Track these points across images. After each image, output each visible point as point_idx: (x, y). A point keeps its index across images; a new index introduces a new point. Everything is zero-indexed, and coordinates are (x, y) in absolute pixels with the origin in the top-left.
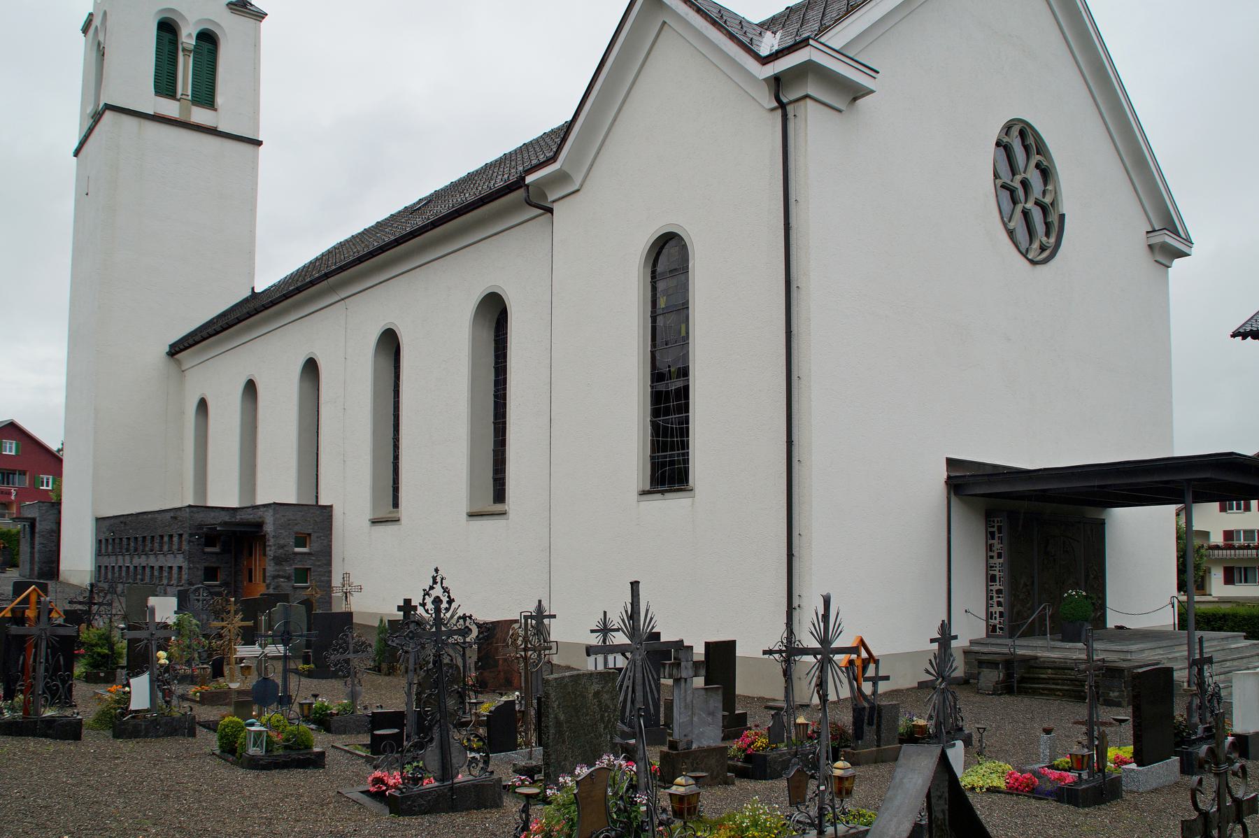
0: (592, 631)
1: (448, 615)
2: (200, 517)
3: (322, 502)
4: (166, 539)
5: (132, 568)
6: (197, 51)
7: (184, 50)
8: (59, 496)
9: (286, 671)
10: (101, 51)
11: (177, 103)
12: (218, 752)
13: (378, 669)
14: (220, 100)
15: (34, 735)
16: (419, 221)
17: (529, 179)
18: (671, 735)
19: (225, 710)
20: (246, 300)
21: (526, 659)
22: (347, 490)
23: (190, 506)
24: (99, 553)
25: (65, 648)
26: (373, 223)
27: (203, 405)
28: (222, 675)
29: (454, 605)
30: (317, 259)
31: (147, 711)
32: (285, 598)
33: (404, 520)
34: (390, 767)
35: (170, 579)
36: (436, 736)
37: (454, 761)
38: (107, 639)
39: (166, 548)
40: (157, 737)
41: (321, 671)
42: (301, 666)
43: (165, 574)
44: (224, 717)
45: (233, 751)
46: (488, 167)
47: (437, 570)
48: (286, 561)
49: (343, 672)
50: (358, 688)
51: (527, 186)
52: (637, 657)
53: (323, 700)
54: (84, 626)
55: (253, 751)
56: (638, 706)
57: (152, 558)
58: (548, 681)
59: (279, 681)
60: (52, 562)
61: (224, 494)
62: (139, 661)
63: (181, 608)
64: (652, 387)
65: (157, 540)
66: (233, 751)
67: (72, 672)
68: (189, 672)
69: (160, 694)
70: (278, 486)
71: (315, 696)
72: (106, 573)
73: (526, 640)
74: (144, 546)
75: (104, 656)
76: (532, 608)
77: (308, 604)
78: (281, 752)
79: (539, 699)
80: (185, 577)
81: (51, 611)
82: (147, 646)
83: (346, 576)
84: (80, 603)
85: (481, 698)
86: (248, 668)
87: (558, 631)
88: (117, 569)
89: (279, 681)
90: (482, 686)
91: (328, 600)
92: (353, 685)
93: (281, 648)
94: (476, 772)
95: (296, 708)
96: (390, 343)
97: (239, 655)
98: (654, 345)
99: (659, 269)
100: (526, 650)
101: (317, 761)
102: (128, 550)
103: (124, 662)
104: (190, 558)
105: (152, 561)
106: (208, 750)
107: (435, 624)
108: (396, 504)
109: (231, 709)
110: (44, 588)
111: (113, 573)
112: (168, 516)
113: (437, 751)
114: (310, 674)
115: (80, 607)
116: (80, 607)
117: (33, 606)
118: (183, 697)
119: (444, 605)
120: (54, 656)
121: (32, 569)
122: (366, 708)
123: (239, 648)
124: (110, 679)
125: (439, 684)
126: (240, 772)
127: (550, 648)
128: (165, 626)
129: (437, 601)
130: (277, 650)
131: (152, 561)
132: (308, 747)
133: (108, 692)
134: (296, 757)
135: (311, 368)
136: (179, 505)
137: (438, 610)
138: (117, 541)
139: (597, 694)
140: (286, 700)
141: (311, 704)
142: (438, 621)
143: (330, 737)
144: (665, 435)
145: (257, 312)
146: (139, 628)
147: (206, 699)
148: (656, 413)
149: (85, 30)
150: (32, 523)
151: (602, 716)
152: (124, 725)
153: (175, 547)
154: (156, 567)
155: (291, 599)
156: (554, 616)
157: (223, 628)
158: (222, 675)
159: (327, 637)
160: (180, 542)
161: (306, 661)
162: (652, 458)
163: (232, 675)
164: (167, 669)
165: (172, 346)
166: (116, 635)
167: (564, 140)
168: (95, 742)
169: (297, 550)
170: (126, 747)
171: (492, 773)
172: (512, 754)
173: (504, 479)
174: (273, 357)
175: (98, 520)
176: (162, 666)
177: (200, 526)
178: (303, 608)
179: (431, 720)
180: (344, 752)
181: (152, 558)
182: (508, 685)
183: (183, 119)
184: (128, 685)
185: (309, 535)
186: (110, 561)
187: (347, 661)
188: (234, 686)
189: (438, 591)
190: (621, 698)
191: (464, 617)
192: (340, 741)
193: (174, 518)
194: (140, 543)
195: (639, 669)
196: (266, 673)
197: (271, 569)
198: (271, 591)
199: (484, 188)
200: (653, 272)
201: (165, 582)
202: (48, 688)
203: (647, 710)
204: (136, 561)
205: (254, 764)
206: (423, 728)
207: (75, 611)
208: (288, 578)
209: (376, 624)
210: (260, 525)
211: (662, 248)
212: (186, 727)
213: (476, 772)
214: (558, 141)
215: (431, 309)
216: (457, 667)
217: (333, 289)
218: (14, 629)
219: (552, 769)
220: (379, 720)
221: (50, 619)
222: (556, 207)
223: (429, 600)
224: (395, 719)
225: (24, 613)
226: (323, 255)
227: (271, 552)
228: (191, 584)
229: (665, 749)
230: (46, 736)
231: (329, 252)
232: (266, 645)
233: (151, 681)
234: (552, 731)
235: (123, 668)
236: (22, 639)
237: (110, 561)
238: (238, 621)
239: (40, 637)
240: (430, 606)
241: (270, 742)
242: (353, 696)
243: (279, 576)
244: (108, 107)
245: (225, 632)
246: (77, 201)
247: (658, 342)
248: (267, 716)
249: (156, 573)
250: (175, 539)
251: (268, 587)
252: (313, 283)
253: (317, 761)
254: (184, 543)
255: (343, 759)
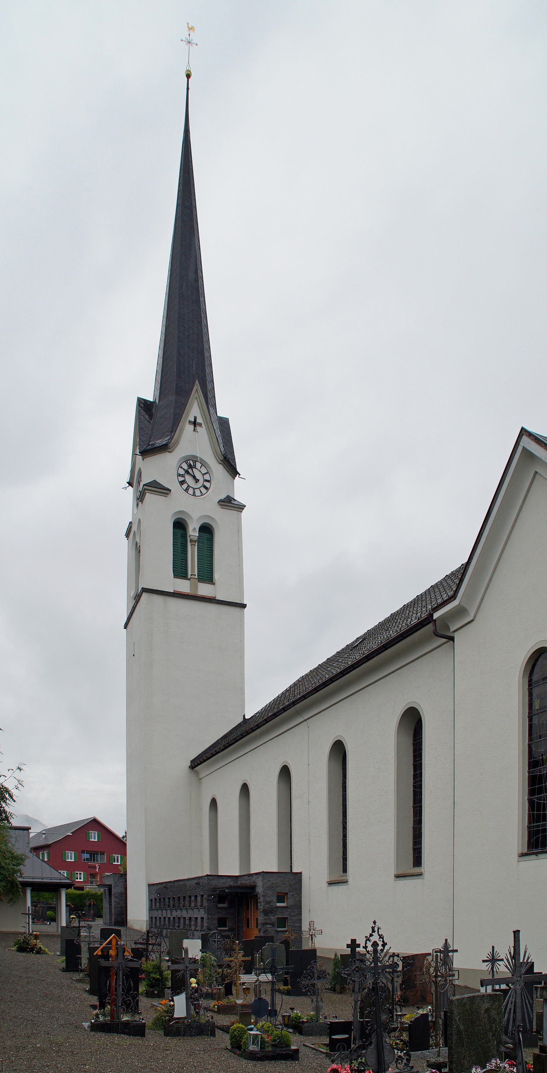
0: (484, 961)
1: (383, 954)
2: (215, 883)
3: (295, 870)
4: (193, 898)
5: (172, 919)
6: (200, 540)
7: (191, 541)
8: (125, 869)
9: (273, 991)
10: (137, 549)
11: (189, 581)
12: (229, 1048)
13: (333, 990)
14: (216, 576)
15: (117, 1033)
16: (358, 656)
17: (436, 616)
18: (541, 1039)
19: (234, 1018)
20: (240, 725)
21: (436, 983)
22: (312, 862)
23: (207, 875)
24: (151, 909)
25: (133, 975)
26: (325, 660)
27: (214, 803)
28: (231, 994)
29: (387, 947)
30: (287, 691)
31: (185, 1018)
32: (271, 939)
33: (350, 881)
34: (343, 1060)
35: (196, 926)
36: (374, 1040)
37: (386, 1058)
38: (158, 968)
39: (193, 904)
40: (191, 1036)
41: (295, 991)
42: (282, 987)
43: (193, 923)
44: (233, 1024)
45: (239, 1047)
46: (405, 607)
47: (375, 922)
48: (271, 913)
49: (311, 991)
50: (321, 1004)
51: (435, 621)
52: (518, 987)
53: (297, 1012)
54: (144, 959)
55: (252, 1048)
56: (518, 1024)
57: (184, 911)
58: (452, 1001)
59: (268, 999)
60: (123, 914)
61: (230, 867)
62: (179, 985)
63: (204, 948)
64: (529, 772)
65: (187, 899)
66: (239, 1047)
67: (138, 991)
68: (210, 991)
69: (192, 1007)
70: (265, 860)
71: (292, 1009)
72: (156, 922)
73: (436, 970)
74: (179, 903)
75: (157, 980)
76: (440, 946)
77: (286, 943)
78: (270, 1049)
79: (445, 1013)
80: (205, 924)
81: (124, 952)
82: (183, 975)
83: (311, 923)
84: (141, 944)
85: (405, 1011)
86: (248, 989)
87: (458, 962)
88: (162, 919)
89: (268, 999)
90: (405, 1002)
91: (299, 940)
92: (317, 1001)
93: (270, 977)
94: (401, 1066)
95: (280, 1018)
96: (339, 751)
97: (242, 981)
98: (530, 739)
99: (535, 678)
100: (436, 976)
101: (293, 1056)
102: (169, 906)
103: (169, 984)
104: (208, 912)
105: (185, 914)
106: (223, 1046)
107: (373, 961)
108: (345, 870)
109: (238, 1018)
110: (118, 933)
111: (160, 922)
112: (194, 882)
113: (375, 1051)
114: (288, 993)
115: (141, 946)
116: (141, 946)
117: (114, 948)
118: (207, 1009)
119: (380, 948)
120: (127, 979)
121: (111, 919)
122: (325, 1018)
123: (242, 976)
124: (161, 995)
125: (376, 1002)
126: (244, 1062)
127: (454, 975)
128: (194, 961)
129: (375, 944)
130: (266, 977)
131: (185, 914)
132: (288, 1046)
133: (160, 1004)
134: (281, 1053)
135: (285, 772)
136: (200, 875)
137: (375, 951)
138: (162, 900)
139: (487, 1010)
140: (273, 1013)
141: (289, 1016)
142: (376, 959)
143: (302, 1038)
144: (538, 810)
145: (248, 733)
146: (178, 963)
147: (222, 1010)
148: (532, 792)
149: (127, 535)
150: (110, 887)
151: (491, 1027)
152: (171, 1027)
153: (199, 904)
154: (187, 918)
155: (275, 939)
156: (456, 951)
157: (231, 961)
158: (231, 994)
159: (299, 968)
160: (202, 900)
161: (286, 984)
162: (529, 827)
163: (238, 994)
164: (196, 990)
165: (192, 762)
166: (164, 965)
167: (461, 580)
168: (154, 1038)
169: (279, 904)
170: (173, 1042)
171: (412, 1067)
172: (426, 1052)
173: (421, 848)
174: (257, 766)
175: (150, 885)
176: (193, 988)
177: (215, 889)
178: (283, 946)
179: (371, 1030)
180: (309, 1046)
181: (184, 911)
182: (423, 1001)
183: (193, 593)
184: (173, 1000)
185: (287, 894)
186: (158, 914)
187: (313, 985)
188: (239, 1002)
189: (375, 938)
190: (506, 1018)
191: (393, 955)
192: (309, 1041)
193: (198, 884)
194: (176, 901)
195: (519, 996)
196: (260, 995)
197: (261, 918)
198: (262, 934)
199: (403, 626)
200: (530, 681)
201: (193, 928)
202: (125, 1002)
203: (524, 1026)
204: (175, 914)
205: (252, 1057)
206: (364, 1035)
207: (138, 949)
208: (273, 925)
209: (333, 957)
210: (253, 887)
211: (536, 660)
212: (208, 1030)
213: (401, 1066)
214: (457, 581)
215: (366, 722)
216: (388, 988)
217: (298, 713)
218: (103, 963)
219: (454, 1065)
220: (334, 1028)
221: (124, 956)
222: (457, 636)
223: (369, 944)
224: (345, 1027)
225: (109, 952)
226: (290, 687)
227: (261, 907)
228: (209, 929)
229: (537, 1051)
230: (124, 1033)
231: (295, 684)
232: (259, 975)
233: (187, 998)
234: (455, 1038)
235: (169, 988)
236: (108, 969)
237: (158, 914)
238: (240, 956)
239: (118, 968)
240: (370, 948)
241: (263, 1042)
242: (317, 1009)
243: (266, 924)
244: (145, 590)
245: (233, 964)
246: (128, 661)
247: (534, 736)
248: (260, 1024)
249: (187, 922)
250: (199, 899)
251: (260, 931)
252: (284, 709)
253: (293, 1056)
254: (205, 901)
255: (311, 1054)
